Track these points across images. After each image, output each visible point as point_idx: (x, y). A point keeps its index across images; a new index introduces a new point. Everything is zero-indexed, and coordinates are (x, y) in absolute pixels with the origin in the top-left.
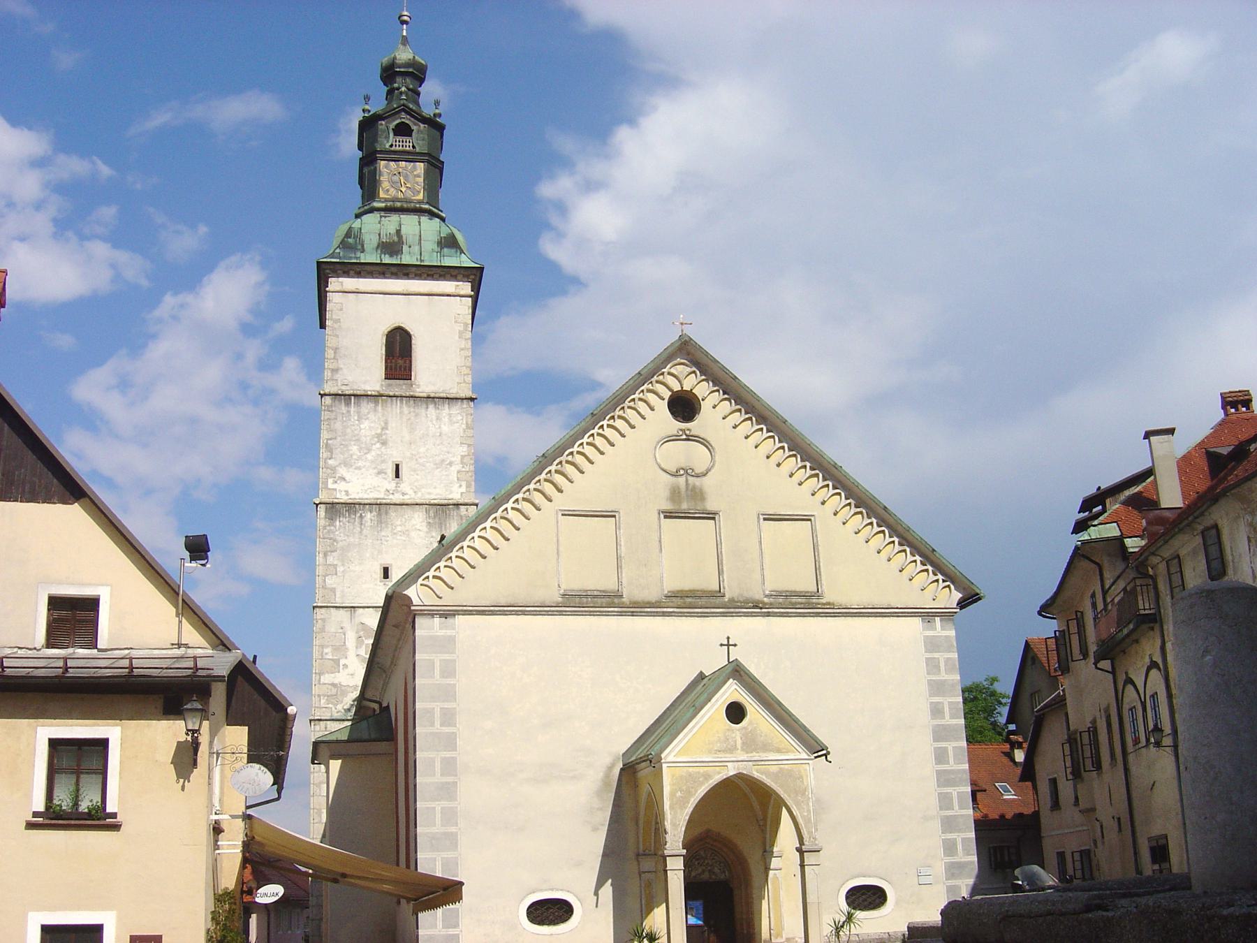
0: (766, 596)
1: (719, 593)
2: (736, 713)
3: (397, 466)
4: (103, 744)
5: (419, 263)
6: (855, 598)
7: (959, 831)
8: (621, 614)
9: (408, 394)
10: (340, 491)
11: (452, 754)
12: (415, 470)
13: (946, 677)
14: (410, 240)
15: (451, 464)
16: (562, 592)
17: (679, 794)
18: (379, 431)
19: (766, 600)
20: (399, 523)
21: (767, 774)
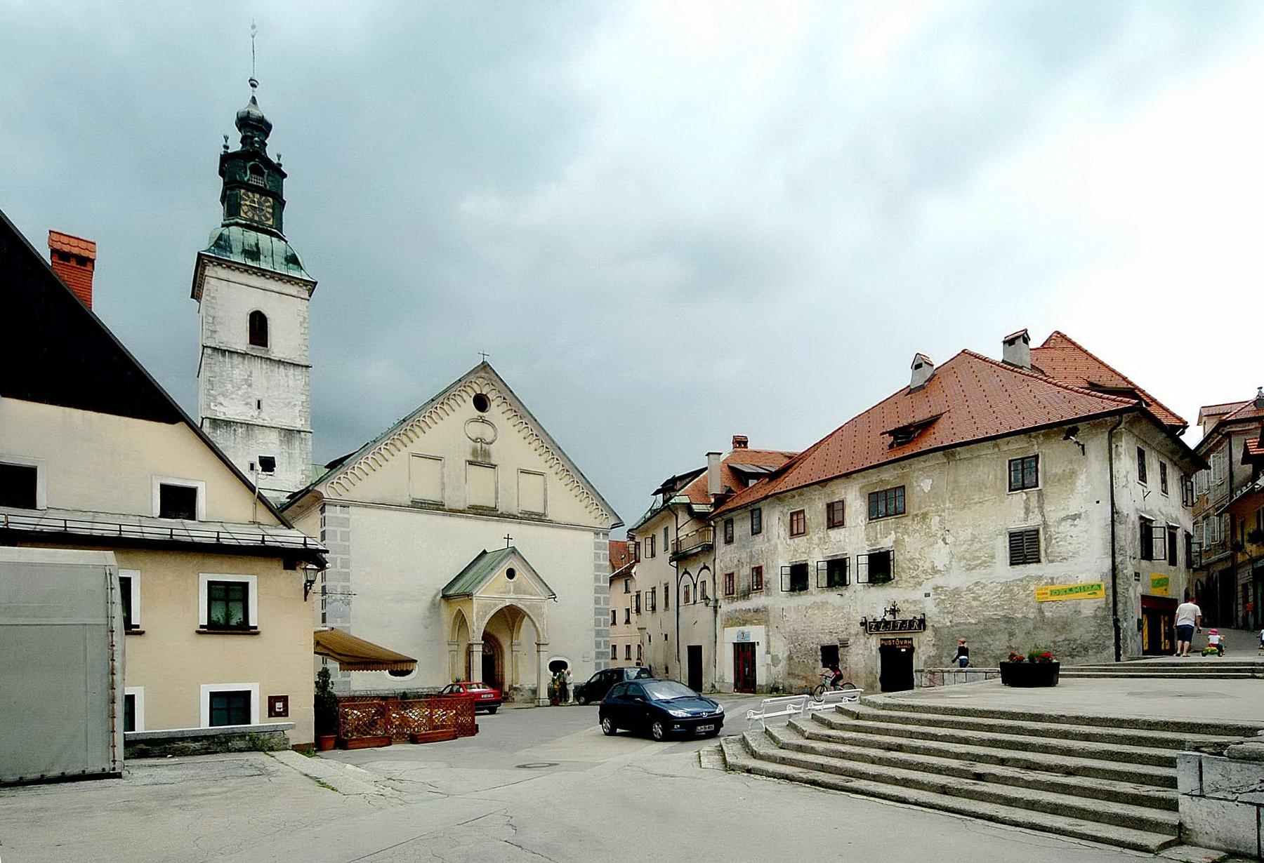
0: (520, 513)
1: (495, 509)
2: (511, 574)
3: (259, 402)
4: (245, 586)
5: (273, 270)
6: (563, 520)
7: (603, 637)
8: (444, 515)
9: (266, 356)
10: (220, 412)
11: (347, 584)
12: (271, 406)
13: (602, 563)
14: (265, 253)
15: (295, 405)
16: (411, 499)
17: (481, 613)
18: (246, 377)
19: (519, 515)
20: (261, 437)
21: (525, 606)
